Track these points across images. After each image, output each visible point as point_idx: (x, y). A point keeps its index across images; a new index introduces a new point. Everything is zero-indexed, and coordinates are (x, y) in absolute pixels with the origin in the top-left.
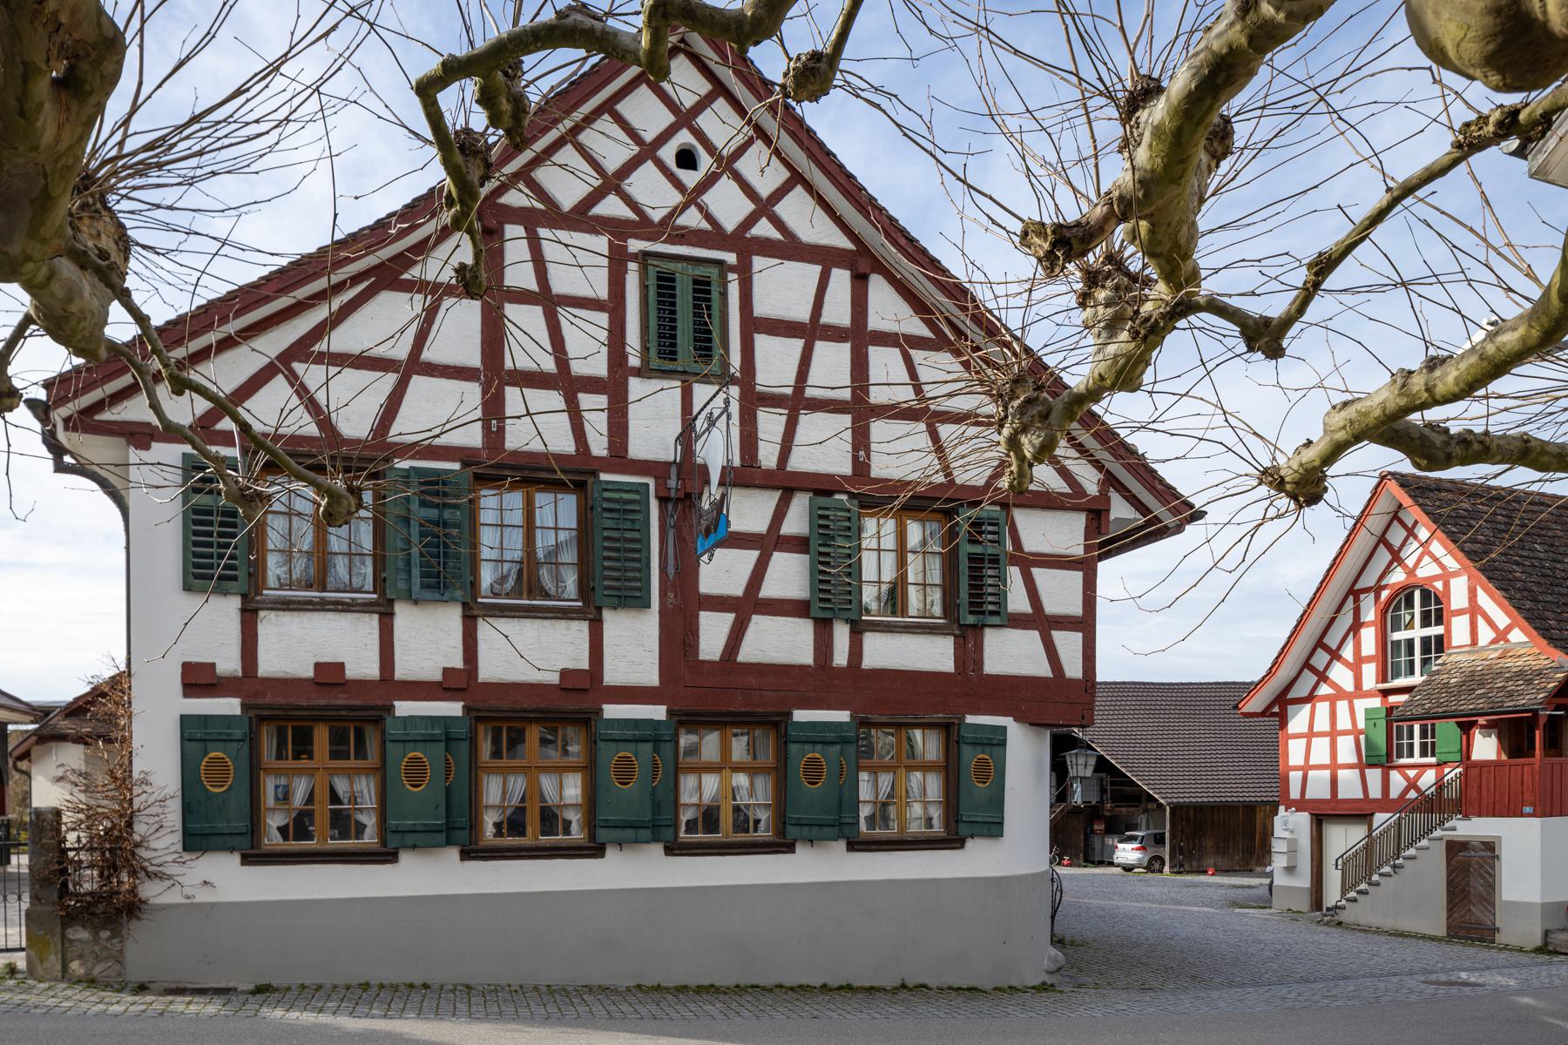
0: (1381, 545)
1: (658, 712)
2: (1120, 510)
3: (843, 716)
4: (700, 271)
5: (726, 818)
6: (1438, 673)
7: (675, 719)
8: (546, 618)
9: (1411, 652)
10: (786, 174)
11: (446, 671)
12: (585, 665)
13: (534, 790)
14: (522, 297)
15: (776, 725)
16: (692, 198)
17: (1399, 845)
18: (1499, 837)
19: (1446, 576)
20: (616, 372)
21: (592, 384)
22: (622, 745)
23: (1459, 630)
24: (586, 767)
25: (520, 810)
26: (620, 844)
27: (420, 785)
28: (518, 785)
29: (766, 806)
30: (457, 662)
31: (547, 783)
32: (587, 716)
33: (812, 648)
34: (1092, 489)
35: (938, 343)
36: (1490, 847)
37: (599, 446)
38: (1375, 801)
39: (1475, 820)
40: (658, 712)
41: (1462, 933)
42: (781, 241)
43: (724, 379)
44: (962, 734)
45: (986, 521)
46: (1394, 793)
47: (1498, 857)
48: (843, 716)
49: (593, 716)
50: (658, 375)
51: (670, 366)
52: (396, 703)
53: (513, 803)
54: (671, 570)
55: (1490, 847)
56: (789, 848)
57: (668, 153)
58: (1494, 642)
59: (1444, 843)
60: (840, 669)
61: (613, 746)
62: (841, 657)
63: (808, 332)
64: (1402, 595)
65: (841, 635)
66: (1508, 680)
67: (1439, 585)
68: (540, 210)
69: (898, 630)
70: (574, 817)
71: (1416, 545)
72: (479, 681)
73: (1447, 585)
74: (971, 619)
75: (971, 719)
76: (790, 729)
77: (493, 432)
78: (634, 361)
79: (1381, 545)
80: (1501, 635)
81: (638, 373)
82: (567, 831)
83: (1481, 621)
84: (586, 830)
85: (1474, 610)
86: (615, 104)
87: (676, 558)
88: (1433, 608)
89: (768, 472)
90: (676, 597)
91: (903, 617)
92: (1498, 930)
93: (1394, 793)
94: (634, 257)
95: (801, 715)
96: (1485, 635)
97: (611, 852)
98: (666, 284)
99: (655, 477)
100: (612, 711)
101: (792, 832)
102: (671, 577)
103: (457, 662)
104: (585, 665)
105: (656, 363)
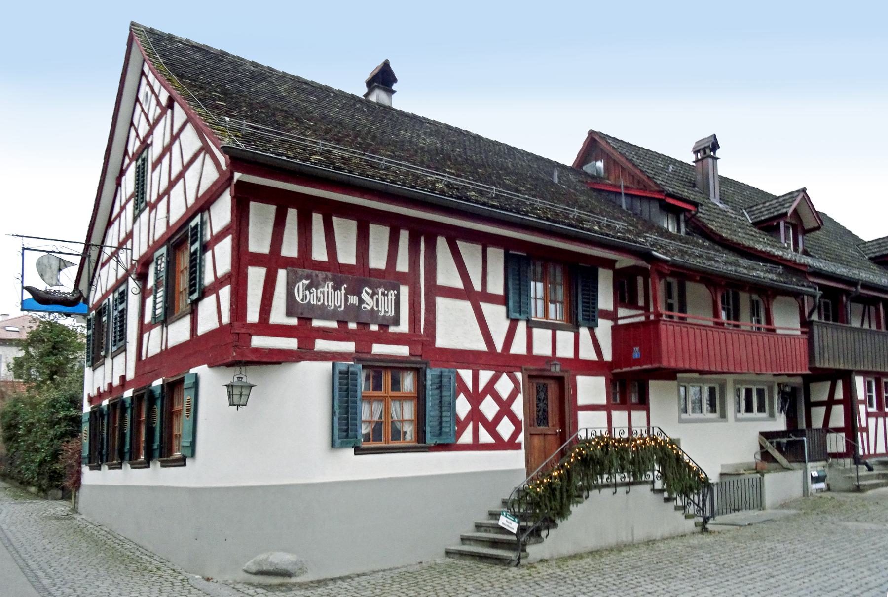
5: (387, 431)
28: (378, 407)
31: (395, 407)
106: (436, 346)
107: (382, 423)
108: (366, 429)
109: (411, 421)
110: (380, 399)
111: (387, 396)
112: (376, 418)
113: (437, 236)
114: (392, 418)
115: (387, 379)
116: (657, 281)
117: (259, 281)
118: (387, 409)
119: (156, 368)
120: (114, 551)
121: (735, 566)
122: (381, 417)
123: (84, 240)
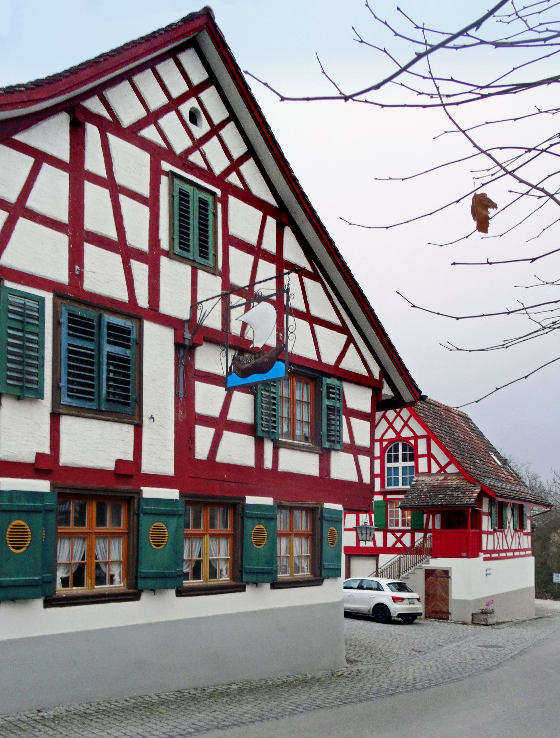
0: (383, 419)
1: (173, 494)
2: (387, 391)
3: (268, 501)
4: (204, 196)
5: (205, 569)
6: (415, 485)
7: (57, 491)
8: (108, 420)
9: (396, 473)
10: (30, 161)
11: (119, 462)
12: (130, 458)
13: (91, 553)
14: (95, 179)
15: (234, 506)
16: (198, 144)
17: (400, 571)
18: (451, 568)
19: (416, 437)
20: (153, 250)
21: (139, 255)
22: (157, 518)
23: (423, 464)
24: (127, 533)
25: (81, 568)
26: (153, 590)
27: (22, 548)
28: (79, 547)
29: (226, 560)
30: (46, 450)
31: (100, 546)
32: (131, 495)
33: (254, 456)
34: (377, 376)
35: (314, 277)
36: (446, 573)
37: (143, 301)
38: (380, 548)
39: (439, 559)
40: (173, 494)
41: (433, 615)
42: (242, 190)
43: (213, 271)
44: (324, 514)
45: (336, 387)
46: (390, 544)
47: (450, 577)
48: (268, 501)
49: (136, 496)
50: (179, 258)
51: (185, 254)
52: (142, 488)
53: (76, 561)
54: (181, 395)
55: (446, 573)
56: (241, 589)
57: (185, 109)
58: (439, 472)
59: (424, 570)
60: (267, 471)
61: (150, 518)
62: (268, 464)
63: (256, 252)
64: (392, 445)
65: (268, 447)
66: (452, 491)
67: (412, 442)
68: (109, 121)
69: (296, 448)
70: (116, 571)
71: (305, 419)
72: (61, 464)
73: (416, 442)
74: (327, 445)
75: (327, 505)
76: (246, 508)
77: (76, 275)
78: (165, 244)
79: (383, 419)
80: (443, 469)
81: (167, 254)
82: (112, 581)
83: (433, 461)
84: (126, 580)
85: (429, 455)
86: (157, 64)
87: (184, 387)
88: (408, 452)
89: (235, 338)
90: (183, 413)
91: (293, 440)
92: (450, 613)
93: (390, 544)
94: (167, 174)
95: (250, 500)
96: (435, 468)
97: (144, 597)
98: (184, 197)
99: (175, 329)
100: (148, 492)
101: (246, 578)
102: (181, 399)
103: (46, 450)
104: (130, 458)
105: (177, 250)
106: (61, 464)
107: (84, 564)
108: (187, 568)
109: (119, 562)
110: (83, 536)
111: (91, 533)
112: (77, 559)
113: (285, 226)
114: (96, 559)
115: (91, 511)
116: (295, 383)
117: (235, 311)
118: (91, 548)
119: (249, 482)
120: (466, 653)
121: (390, 639)
122: (83, 559)
123: (403, 65)
